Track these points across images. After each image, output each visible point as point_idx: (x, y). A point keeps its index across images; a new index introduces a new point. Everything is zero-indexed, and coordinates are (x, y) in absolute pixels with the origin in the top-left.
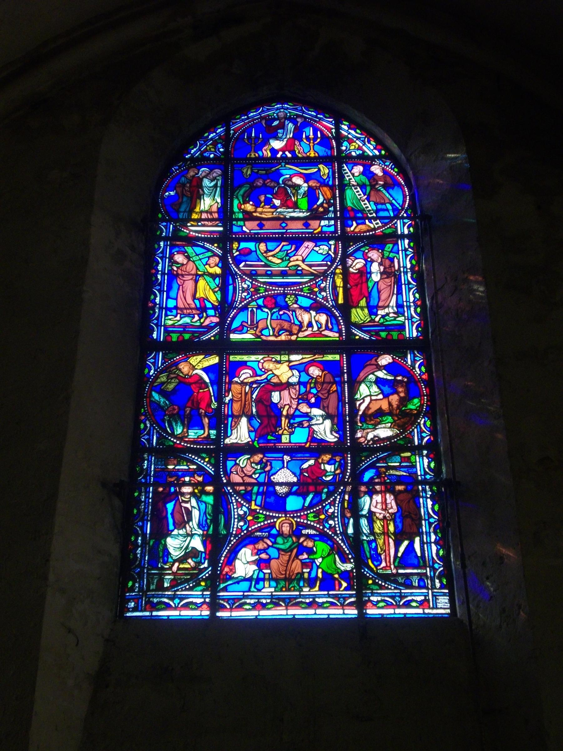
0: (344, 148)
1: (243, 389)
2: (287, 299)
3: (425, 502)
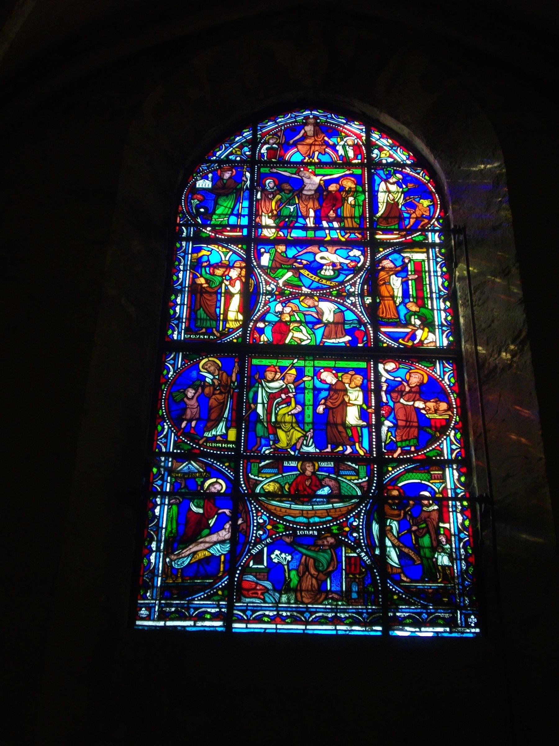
0: (374, 156)
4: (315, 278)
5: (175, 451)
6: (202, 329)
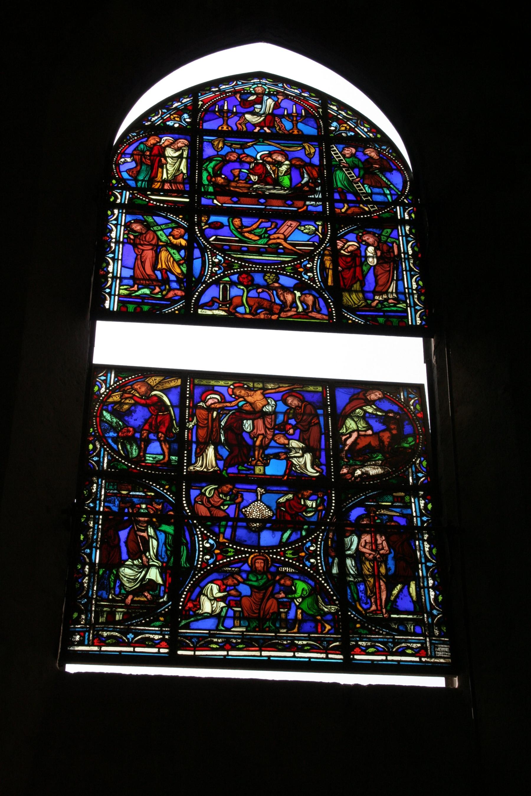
1: (210, 415)
2: (266, 278)
3: (421, 545)
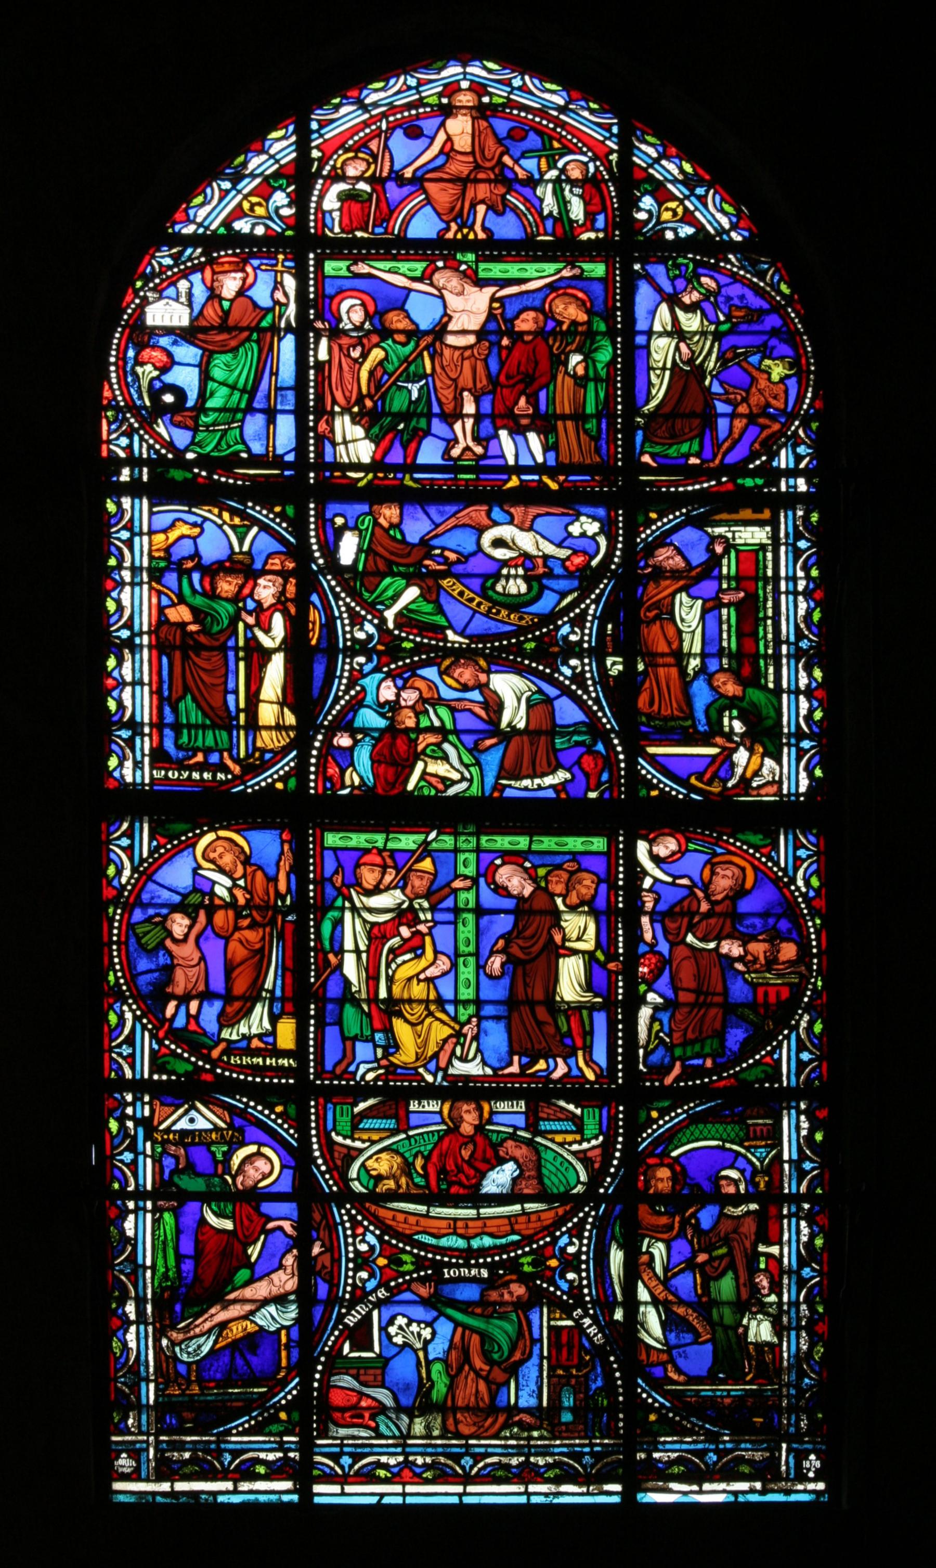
4: (479, 604)
5: (156, 1077)
6: (195, 755)
